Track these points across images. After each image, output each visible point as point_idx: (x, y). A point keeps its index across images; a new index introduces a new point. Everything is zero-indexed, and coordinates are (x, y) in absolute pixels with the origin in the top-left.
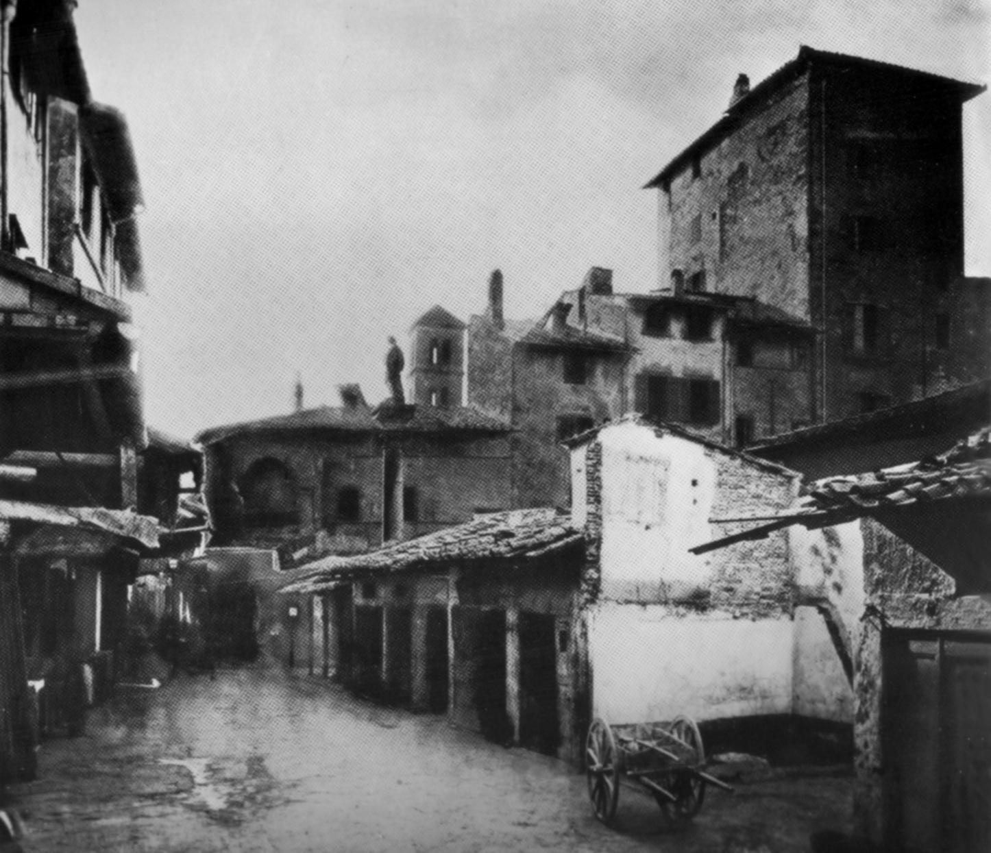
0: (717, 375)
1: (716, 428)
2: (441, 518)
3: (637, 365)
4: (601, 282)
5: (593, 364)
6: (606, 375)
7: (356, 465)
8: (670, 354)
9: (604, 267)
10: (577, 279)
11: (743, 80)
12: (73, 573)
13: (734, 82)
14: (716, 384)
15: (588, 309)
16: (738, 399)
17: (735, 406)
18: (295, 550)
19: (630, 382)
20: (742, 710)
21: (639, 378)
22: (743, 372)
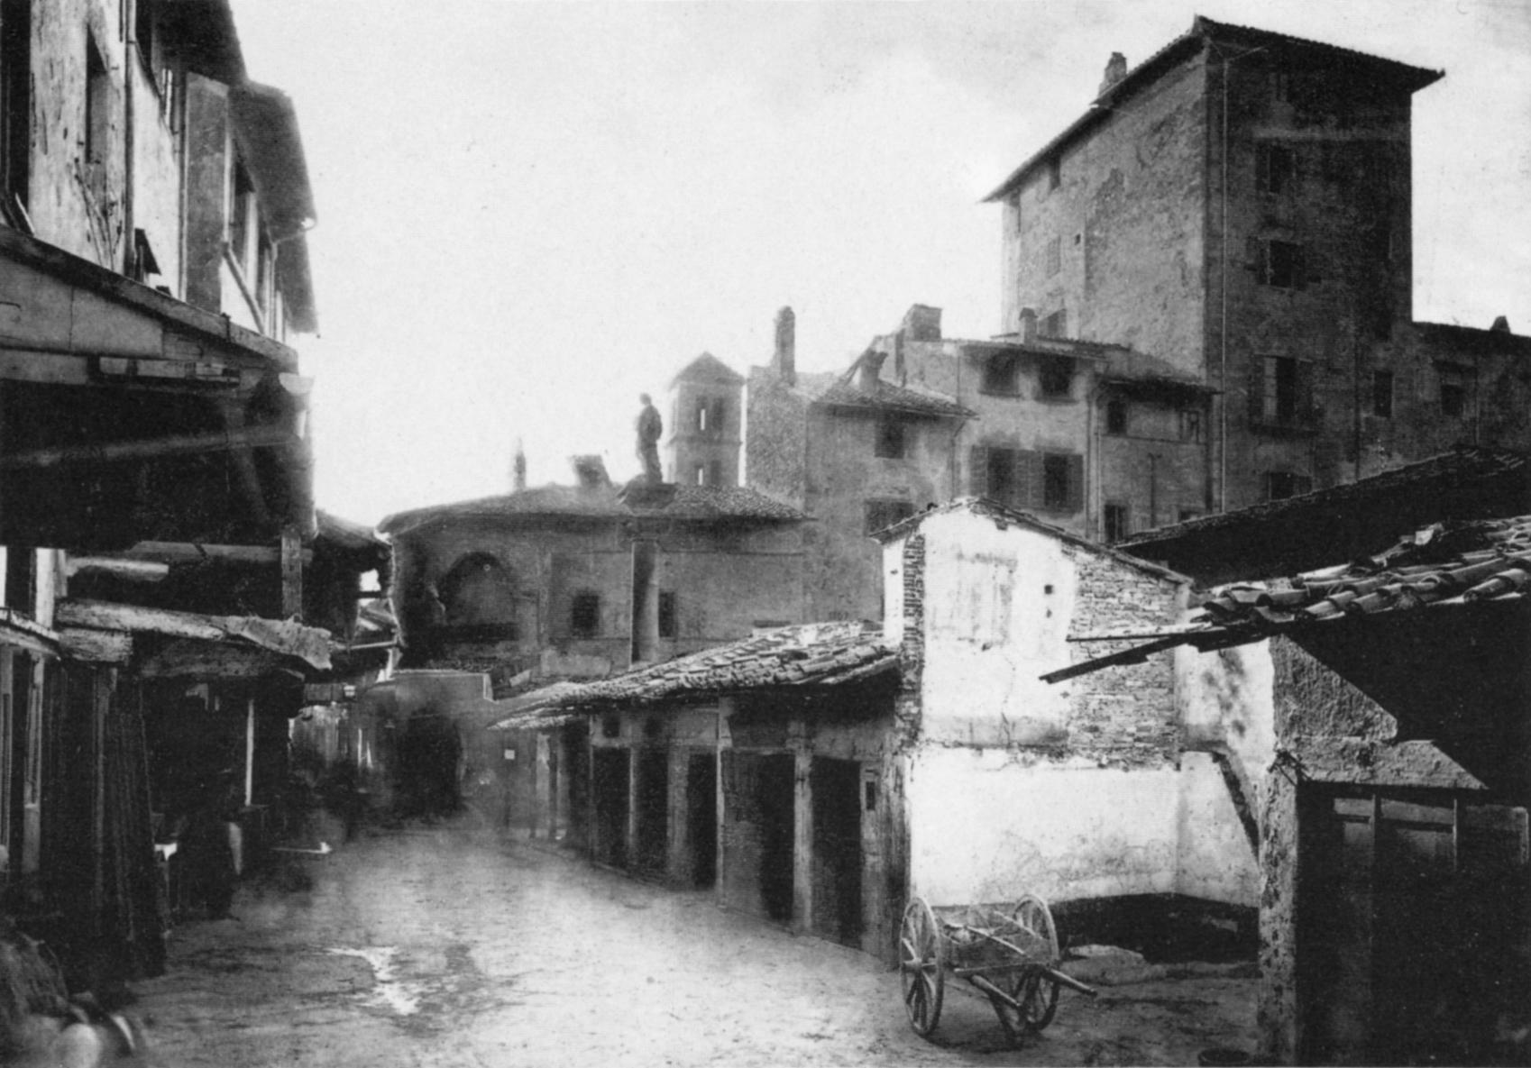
0: (1080, 448)
1: (1079, 517)
2: (710, 633)
3: (973, 434)
8: (1027, 422)
9: (931, 304)
11: (1118, 60)
12: (100, 850)
13: (1105, 63)
14: (1079, 458)
19: (963, 456)
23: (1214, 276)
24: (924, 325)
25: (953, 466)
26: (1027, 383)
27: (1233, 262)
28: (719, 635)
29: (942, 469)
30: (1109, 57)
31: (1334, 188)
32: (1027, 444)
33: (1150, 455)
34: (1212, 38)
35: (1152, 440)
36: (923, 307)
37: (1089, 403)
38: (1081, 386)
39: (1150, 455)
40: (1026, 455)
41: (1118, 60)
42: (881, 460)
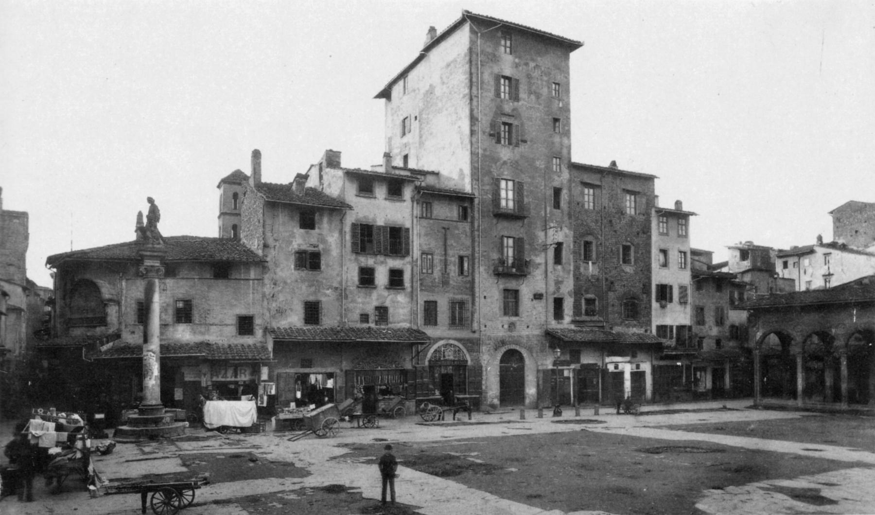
0: (408, 225)
1: (408, 259)
2: (210, 320)
3: (350, 219)
4: (332, 160)
5: (321, 215)
6: (330, 222)
7: (553, 143)
8: (382, 210)
9: (335, 149)
10: (318, 157)
11: (432, 30)
12: (758, 338)
13: (427, 31)
14: (407, 230)
15: (325, 177)
16: (422, 240)
17: (420, 245)
18: (102, 344)
19: (348, 229)
20: (208, 411)
21: (354, 226)
22: (425, 222)
23: (474, 140)
24: (332, 160)
25: (341, 232)
26: (381, 192)
27: (484, 133)
28: (216, 321)
29: (336, 235)
30: (428, 28)
31: (533, 97)
32: (380, 222)
33: (444, 228)
34: (468, 18)
35: (842, 265)
36: (331, 151)
37: (413, 201)
38: (408, 192)
39: (444, 228)
40: (379, 228)
41: (432, 30)
42: (302, 231)
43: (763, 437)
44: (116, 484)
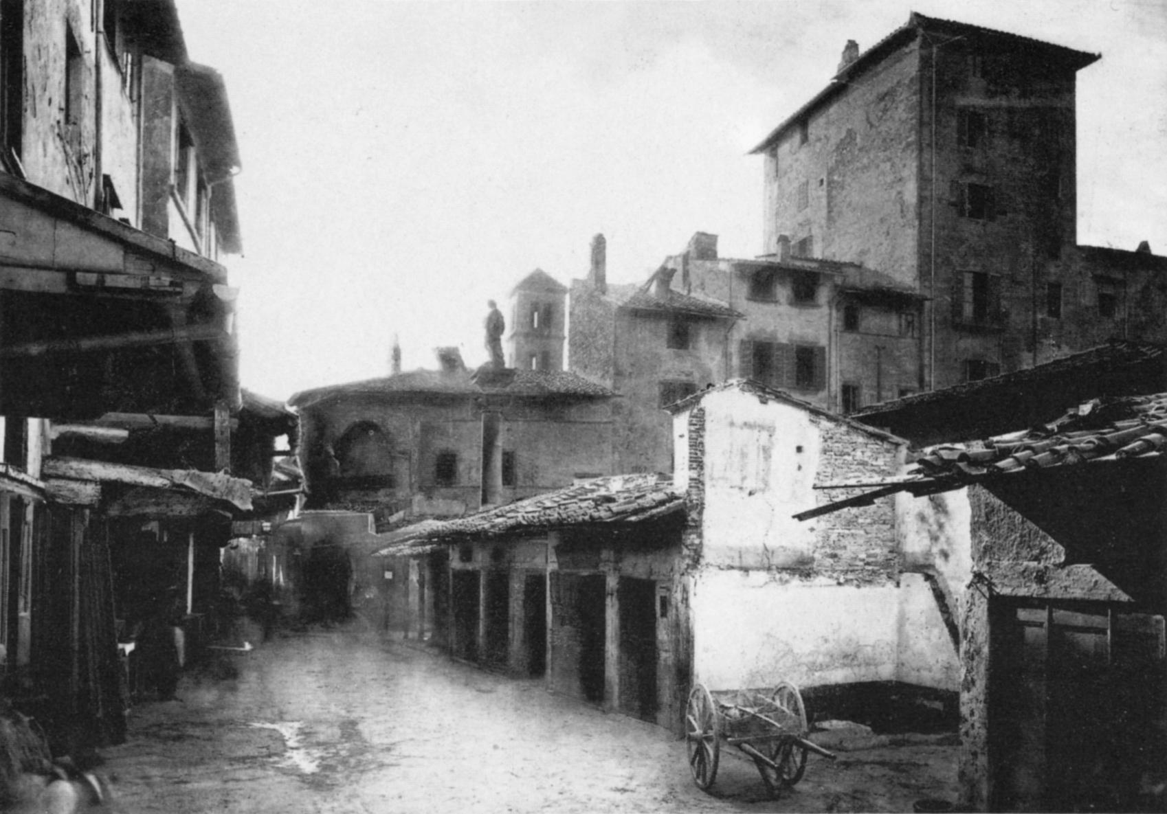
0: (823, 342)
1: (823, 394)
2: (541, 482)
3: (742, 331)
8: (783, 322)
9: (710, 232)
11: (852, 45)
12: (77, 648)
13: (842, 48)
14: (822, 349)
19: (734, 348)
23: (925, 210)
24: (705, 247)
25: (726, 355)
26: (783, 292)
27: (940, 200)
28: (548, 484)
29: (718, 358)
30: (845, 43)
31: (1017, 143)
32: (783, 338)
33: (877, 347)
36: (704, 234)
37: (830, 307)
38: (824, 294)
39: (877, 347)
40: (782, 347)
41: (852, 45)
42: (671, 351)
43: (506, 621)
44: (193, 370)
